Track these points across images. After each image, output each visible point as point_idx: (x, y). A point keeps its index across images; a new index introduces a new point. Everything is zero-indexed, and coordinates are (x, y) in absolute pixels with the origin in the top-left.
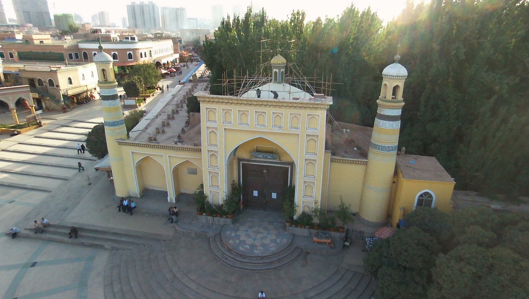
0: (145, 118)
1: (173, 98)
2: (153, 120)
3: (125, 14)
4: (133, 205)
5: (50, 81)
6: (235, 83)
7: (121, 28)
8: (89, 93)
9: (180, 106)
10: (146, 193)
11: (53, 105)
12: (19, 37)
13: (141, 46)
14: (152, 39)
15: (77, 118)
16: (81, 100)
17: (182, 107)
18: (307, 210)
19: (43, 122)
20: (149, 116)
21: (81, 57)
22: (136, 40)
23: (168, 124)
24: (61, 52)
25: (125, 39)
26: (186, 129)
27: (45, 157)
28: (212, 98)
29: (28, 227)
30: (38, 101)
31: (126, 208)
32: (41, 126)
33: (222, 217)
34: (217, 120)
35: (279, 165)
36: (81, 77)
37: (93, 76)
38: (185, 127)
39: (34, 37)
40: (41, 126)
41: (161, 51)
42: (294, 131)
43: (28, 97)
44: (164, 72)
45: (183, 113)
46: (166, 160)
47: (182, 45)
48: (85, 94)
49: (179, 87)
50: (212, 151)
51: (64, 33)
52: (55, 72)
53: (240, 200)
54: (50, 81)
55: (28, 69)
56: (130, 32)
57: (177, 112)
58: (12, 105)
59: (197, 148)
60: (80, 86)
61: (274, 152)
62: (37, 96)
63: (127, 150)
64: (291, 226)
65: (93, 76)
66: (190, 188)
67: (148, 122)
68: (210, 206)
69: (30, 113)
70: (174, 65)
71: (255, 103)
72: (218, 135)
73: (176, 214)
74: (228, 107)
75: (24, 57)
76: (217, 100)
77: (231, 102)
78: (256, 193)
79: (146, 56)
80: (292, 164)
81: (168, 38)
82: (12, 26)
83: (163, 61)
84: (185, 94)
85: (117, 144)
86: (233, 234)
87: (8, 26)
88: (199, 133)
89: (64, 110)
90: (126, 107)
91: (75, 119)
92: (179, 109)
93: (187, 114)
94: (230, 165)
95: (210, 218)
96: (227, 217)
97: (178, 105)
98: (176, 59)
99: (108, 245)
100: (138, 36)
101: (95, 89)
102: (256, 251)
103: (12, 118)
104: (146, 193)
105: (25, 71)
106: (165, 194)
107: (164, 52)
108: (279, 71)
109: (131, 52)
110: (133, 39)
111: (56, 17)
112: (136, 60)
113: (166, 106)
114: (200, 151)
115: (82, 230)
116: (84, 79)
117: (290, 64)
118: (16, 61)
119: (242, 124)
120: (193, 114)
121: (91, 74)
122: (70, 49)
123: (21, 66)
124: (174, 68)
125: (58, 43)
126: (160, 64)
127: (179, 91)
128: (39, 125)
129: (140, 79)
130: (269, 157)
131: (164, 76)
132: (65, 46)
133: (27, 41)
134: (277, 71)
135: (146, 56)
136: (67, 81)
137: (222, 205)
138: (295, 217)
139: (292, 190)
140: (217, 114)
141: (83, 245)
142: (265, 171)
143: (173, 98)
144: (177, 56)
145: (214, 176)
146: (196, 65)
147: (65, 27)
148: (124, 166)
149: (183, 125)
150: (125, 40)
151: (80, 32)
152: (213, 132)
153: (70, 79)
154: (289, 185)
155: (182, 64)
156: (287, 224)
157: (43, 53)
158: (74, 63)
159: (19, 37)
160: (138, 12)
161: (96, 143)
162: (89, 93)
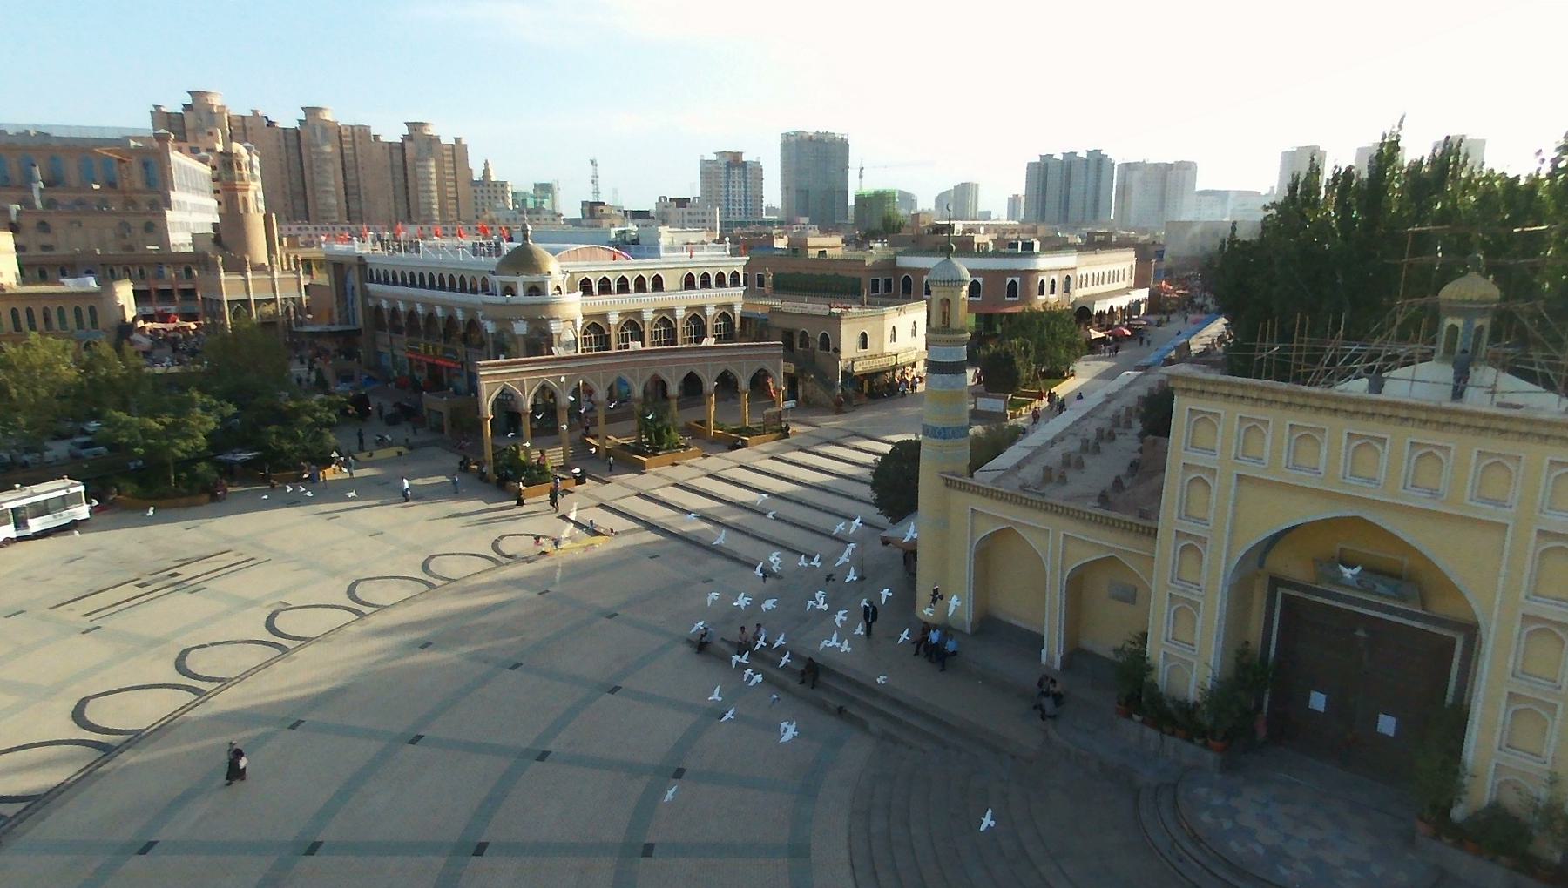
0: (1019, 444)
1: (1108, 402)
2: (1038, 451)
3: (1018, 185)
4: (951, 646)
5: (824, 336)
6: (1294, 354)
7: (1004, 221)
8: (898, 373)
9: (1122, 423)
10: (988, 625)
11: (820, 393)
12: (781, 243)
13: (1047, 264)
14: (1080, 249)
15: (866, 429)
16: (880, 388)
17: (1129, 425)
18: (1511, 800)
19: (794, 428)
20: (1035, 439)
21: (896, 287)
22: (1037, 248)
23: (1080, 465)
24: (857, 275)
25: (1007, 245)
26: (1127, 483)
27: (781, 502)
28: (1213, 383)
29: (729, 638)
30: (792, 381)
31: (934, 650)
32: (787, 436)
33: (1190, 740)
34: (1218, 446)
35: (1417, 625)
36: (888, 332)
37: (914, 333)
38: (1127, 476)
39: (811, 241)
40: (787, 436)
41: (1099, 279)
42: (1487, 512)
43: (777, 369)
44: (1096, 334)
45: (1128, 444)
46: (1057, 544)
47: (1163, 266)
48: (889, 375)
49: (1129, 375)
50: (1189, 535)
51: (871, 235)
52: (838, 317)
53: (1259, 707)
54: (824, 336)
55: (788, 310)
56: (1023, 231)
57: (1112, 437)
58: (744, 384)
59: (1148, 523)
60: (883, 355)
61: (1404, 575)
62: (792, 369)
63: (964, 502)
64: (1437, 837)
65: (914, 333)
66: (1106, 639)
67: (1027, 452)
68: (1157, 698)
69: (773, 404)
70: (1130, 319)
71: (1351, 408)
72: (1214, 491)
73: (1058, 698)
74: (1260, 413)
75: (787, 285)
76: (1226, 390)
77: (1270, 397)
78: (1318, 701)
79: (1052, 292)
80: (1471, 631)
81: (1123, 244)
82: (771, 223)
83: (1099, 307)
84: (1145, 393)
85: (942, 482)
86: (1218, 801)
87: (763, 223)
88: (1158, 493)
89: (839, 408)
90: (977, 416)
91: (856, 429)
92: (1116, 430)
93: (1136, 445)
94: (1240, 590)
95: (1151, 733)
96: (1206, 745)
97: (1116, 420)
98: (1138, 303)
99: (875, 724)
100: (1043, 241)
101: (914, 365)
102: (1284, 872)
103: (739, 411)
104: (988, 625)
105: (779, 312)
106: (1036, 641)
107: (1107, 280)
108: (1468, 323)
109: (1017, 280)
110: (1028, 246)
111: (858, 198)
112: (1027, 298)
113: (1083, 418)
114: (1152, 533)
115: (830, 672)
116: (894, 338)
117: (1521, 306)
118: (767, 292)
119: (1296, 467)
120: (1155, 442)
121: (911, 327)
122: (880, 267)
123: (776, 303)
124: (1128, 328)
125: (855, 254)
126: (1090, 315)
127: (1128, 386)
128: (784, 433)
129: (1026, 346)
130: (1381, 588)
131: (1093, 347)
132: (869, 262)
133: (795, 251)
134: (1459, 322)
135: (1052, 292)
136: (856, 340)
137: (1196, 705)
138: (1458, 813)
139: (1459, 719)
140: (1220, 429)
141: (823, 707)
142: (1361, 633)
143: (1108, 402)
144: (1143, 294)
145: (1184, 610)
146: (1195, 322)
147: (880, 218)
148: (946, 528)
149: (1122, 471)
150: (1007, 250)
151: (905, 232)
152: (1200, 480)
153: (864, 335)
154: (1449, 699)
155: (1153, 318)
156: (1421, 827)
157: (823, 276)
158: (879, 300)
159: (781, 243)
160: (1054, 181)
161: (895, 484)
162: (898, 373)
